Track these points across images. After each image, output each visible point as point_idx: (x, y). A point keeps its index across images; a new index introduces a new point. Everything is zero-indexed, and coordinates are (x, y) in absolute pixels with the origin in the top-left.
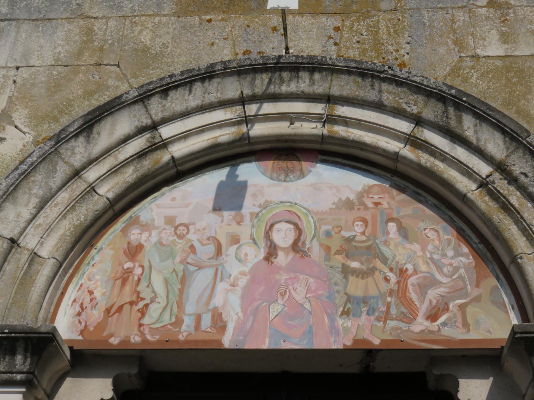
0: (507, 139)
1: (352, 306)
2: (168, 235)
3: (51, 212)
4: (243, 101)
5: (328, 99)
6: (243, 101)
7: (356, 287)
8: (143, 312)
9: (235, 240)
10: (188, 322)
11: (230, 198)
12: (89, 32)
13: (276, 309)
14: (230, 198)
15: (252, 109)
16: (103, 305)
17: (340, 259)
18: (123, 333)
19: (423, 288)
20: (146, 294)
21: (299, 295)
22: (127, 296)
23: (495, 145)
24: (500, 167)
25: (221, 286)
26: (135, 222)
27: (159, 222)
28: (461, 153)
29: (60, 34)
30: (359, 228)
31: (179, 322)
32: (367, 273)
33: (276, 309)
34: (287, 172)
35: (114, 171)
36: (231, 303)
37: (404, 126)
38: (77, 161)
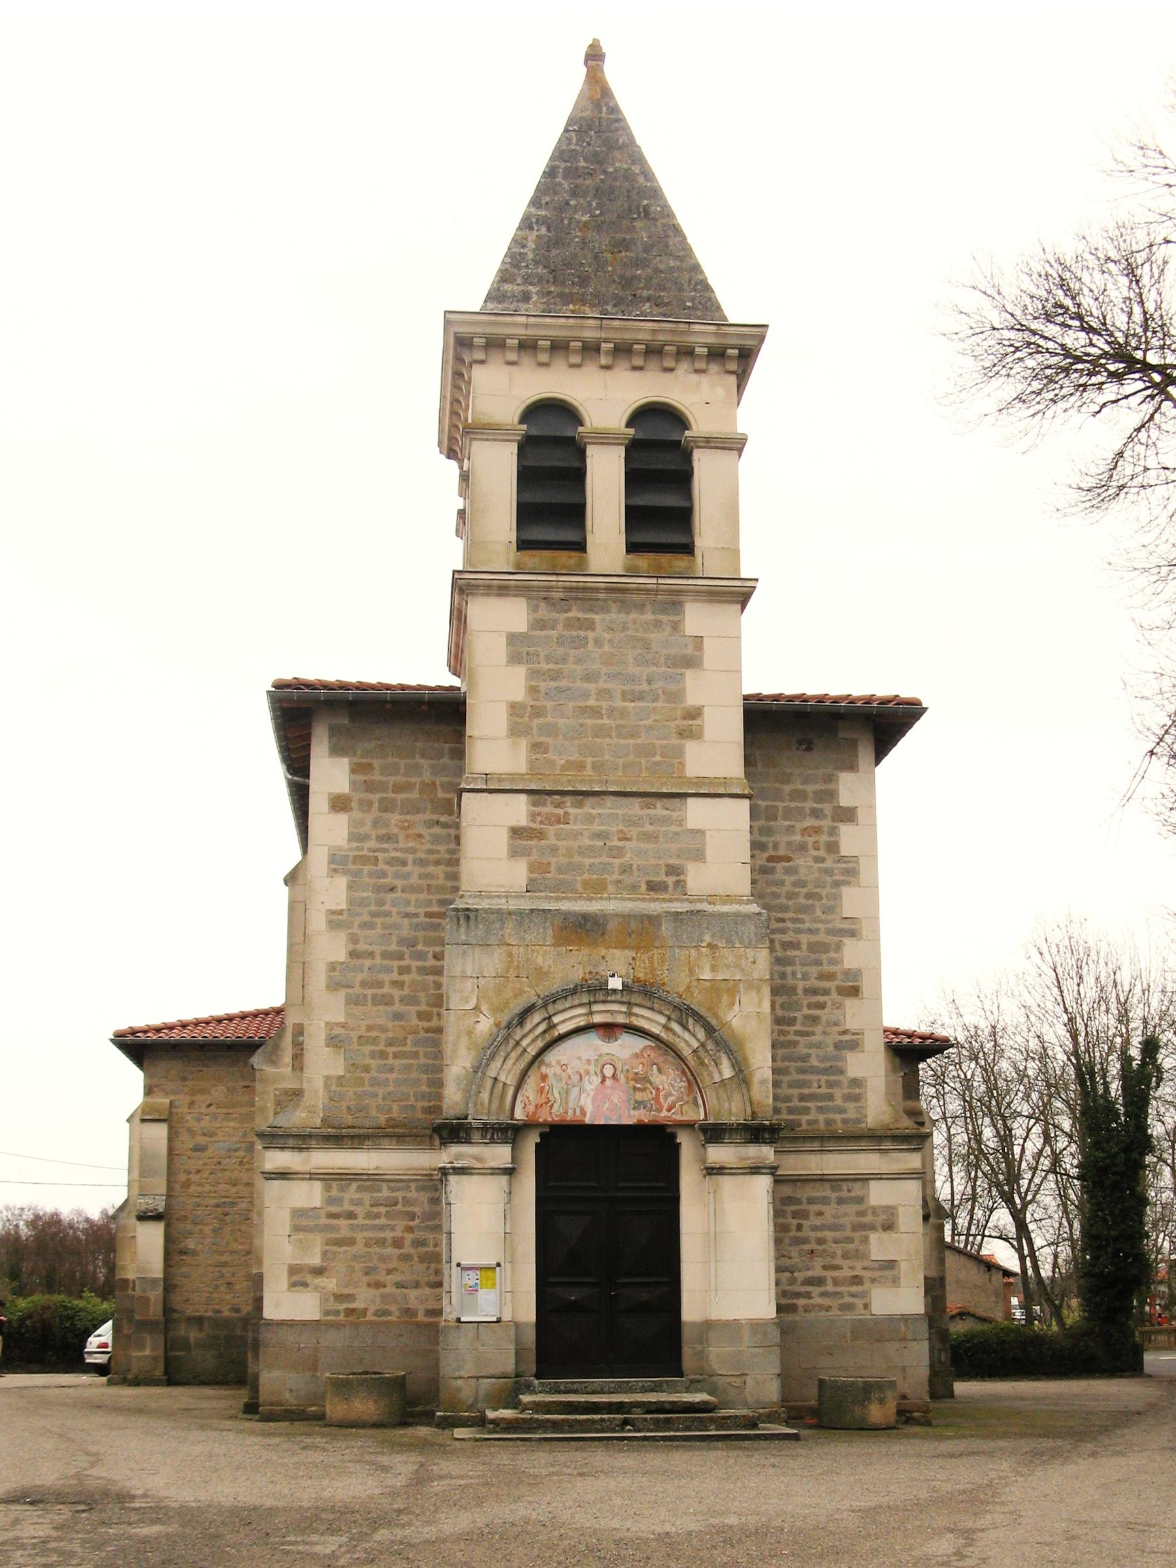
0: (841, 735)
1: (638, 1105)
2: (558, 1070)
3: (510, 1063)
7: (639, 1096)
9: (588, 1073)
12: (510, 955)
13: (606, 1106)
18: (544, 1116)
21: (616, 1101)
25: (583, 1096)
28: (686, 1035)
31: (566, 1112)
33: (606, 1106)
35: (534, 1040)
36: (587, 1103)
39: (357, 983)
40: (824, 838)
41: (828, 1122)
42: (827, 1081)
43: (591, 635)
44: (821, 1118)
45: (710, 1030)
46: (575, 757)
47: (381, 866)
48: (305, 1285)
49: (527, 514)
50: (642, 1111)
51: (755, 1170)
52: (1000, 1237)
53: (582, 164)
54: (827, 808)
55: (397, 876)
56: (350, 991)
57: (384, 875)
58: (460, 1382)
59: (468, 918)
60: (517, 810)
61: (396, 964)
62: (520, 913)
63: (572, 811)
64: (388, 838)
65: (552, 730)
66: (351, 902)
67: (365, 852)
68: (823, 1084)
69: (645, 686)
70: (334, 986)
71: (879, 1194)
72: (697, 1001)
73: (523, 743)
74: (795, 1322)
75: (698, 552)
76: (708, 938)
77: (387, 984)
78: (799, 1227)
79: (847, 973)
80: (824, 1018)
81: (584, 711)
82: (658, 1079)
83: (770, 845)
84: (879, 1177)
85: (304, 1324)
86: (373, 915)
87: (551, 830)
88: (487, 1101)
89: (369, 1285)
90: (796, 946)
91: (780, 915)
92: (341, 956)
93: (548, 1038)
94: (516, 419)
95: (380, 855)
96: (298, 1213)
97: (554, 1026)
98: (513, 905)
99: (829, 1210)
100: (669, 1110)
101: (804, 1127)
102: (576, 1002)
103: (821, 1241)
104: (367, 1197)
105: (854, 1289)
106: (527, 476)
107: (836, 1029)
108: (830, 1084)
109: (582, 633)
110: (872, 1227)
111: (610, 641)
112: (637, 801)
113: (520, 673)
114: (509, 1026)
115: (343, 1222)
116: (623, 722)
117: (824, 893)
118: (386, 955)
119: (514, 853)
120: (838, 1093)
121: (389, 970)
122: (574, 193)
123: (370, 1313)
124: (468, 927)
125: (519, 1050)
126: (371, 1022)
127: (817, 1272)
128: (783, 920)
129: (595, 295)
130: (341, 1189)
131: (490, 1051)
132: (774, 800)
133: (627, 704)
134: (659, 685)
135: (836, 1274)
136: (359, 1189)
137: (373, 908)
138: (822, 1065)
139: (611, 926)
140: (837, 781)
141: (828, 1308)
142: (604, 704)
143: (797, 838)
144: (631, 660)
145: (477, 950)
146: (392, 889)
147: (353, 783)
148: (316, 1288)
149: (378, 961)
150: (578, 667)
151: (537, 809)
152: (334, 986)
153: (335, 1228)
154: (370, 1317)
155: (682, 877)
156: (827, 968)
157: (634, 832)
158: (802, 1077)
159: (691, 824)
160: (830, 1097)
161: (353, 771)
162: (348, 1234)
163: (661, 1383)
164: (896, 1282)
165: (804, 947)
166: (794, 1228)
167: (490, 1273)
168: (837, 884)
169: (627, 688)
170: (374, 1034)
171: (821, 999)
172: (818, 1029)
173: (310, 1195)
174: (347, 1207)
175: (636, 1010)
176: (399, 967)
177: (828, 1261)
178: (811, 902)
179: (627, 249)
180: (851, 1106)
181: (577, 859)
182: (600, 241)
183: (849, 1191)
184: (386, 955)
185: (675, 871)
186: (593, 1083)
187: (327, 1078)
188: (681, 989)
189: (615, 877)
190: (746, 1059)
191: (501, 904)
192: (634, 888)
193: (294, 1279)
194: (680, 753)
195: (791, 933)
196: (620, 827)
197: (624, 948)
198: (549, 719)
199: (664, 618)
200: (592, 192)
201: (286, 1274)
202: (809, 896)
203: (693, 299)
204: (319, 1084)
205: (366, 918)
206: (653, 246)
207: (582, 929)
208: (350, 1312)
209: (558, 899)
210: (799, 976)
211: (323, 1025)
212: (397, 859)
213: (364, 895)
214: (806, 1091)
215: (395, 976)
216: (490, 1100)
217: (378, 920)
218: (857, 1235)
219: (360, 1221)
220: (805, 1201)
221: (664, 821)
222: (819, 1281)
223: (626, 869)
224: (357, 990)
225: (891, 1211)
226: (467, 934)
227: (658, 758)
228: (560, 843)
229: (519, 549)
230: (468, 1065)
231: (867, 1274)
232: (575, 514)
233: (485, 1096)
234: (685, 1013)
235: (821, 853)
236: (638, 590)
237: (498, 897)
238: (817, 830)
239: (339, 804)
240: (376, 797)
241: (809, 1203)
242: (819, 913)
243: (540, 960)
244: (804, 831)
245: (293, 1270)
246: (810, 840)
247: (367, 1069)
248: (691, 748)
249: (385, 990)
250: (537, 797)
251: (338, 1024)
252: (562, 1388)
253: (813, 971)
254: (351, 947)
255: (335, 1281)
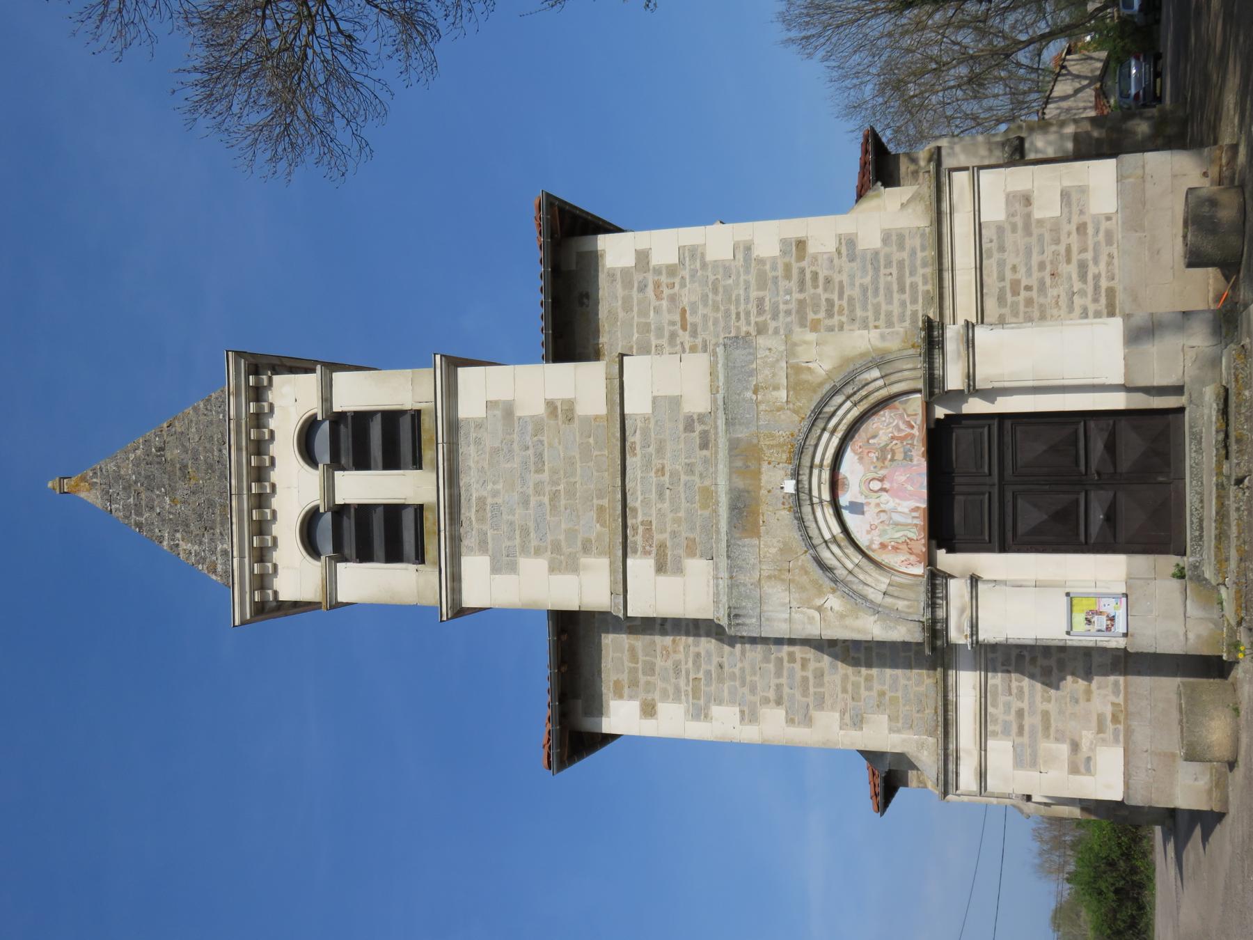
0: (574, 267)
1: (907, 457)
2: (876, 532)
3: (869, 580)
4: (812, 504)
5: (811, 467)
6: (812, 504)
7: (899, 456)
8: (911, 540)
9: (878, 505)
10: (915, 521)
11: (857, 508)
12: (769, 577)
13: (910, 488)
14: (857, 508)
15: (815, 500)
16: (908, 556)
17: (887, 463)
18: (921, 546)
19: (900, 430)
20: (903, 539)
21: (903, 478)
22: (904, 546)
23: (839, 399)
24: (848, 398)
25: (899, 509)
26: (869, 547)
27: (869, 537)
28: (840, 413)
29: (770, 591)
30: (872, 455)
31: (916, 525)
32: (893, 451)
33: (910, 488)
34: (844, 484)
35: (848, 556)
36: (906, 506)
37: (826, 435)
38: (845, 572)
39: (804, 699)
40: (664, 279)
41: (924, 265)
42: (885, 267)
43: (489, 501)
44: (921, 271)
45: (835, 391)
46: (593, 514)
47: (701, 675)
48: (1089, 759)
49: (394, 555)
50: (914, 453)
51: (970, 343)
52: (1039, 55)
53: (131, 500)
54: (637, 277)
55: (709, 661)
56: (811, 707)
57: (708, 673)
58: (1191, 636)
59: (736, 616)
60: (641, 567)
61: (786, 664)
62: (730, 569)
63: (640, 519)
64: (677, 671)
65: (571, 534)
66: (732, 702)
67: (690, 689)
68: (888, 271)
69: (531, 452)
70: (808, 721)
71: (994, 211)
72: (808, 404)
73: (584, 560)
74: (1125, 289)
75: (417, 406)
76: (749, 394)
77: (804, 674)
78: (1028, 288)
79: (784, 252)
80: (826, 273)
81: (554, 507)
82: (883, 438)
83: (672, 328)
84: (977, 212)
85: (1127, 764)
86: (743, 684)
87: (658, 537)
88: (906, 603)
89: (1088, 700)
90: (760, 302)
91: (734, 317)
92: (780, 713)
93: (844, 543)
94: (318, 564)
95: (692, 676)
96: (1019, 763)
97: (834, 537)
98: (724, 574)
99: (1011, 259)
100: (912, 427)
101: (929, 287)
102: (811, 517)
103: (1042, 266)
104: (1002, 699)
105: (1090, 231)
106: (364, 555)
107: (836, 261)
108: (889, 264)
109: (488, 508)
110: (1028, 216)
111: (494, 483)
112: (630, 460)
113: (525, 563)
114: (835, 581)
115: (1027, 722)
116: (562, 472)
117: (712, 278)
118: (779, 674)
119: (679, 570)
120: (897, 256)
121: (792, 671)
122: (152, 508)
123: (1117, 701)
124: (744, 616)
125: (856, 571)
126: (839, 689)
127: (1073, 269)
128: (738, 314)
129: (221, 494)
130: (995, 721)
131: (856, 598)
132: (632, 325)
133: (546, 468)
134: (529, 440)
135: (1075, 249)
136: (995, 706)
137: (737, 683)
138: (870, 273)
139: (740, 483)
140: (614, 269)
141: (1110, 256)
142: (547, 489)
143: (665, 303)
144: (508, 465)
145: (765, 608)
146: (721, 666)
147: (631, 698)
148: (1092, 749)
149: (784, 680)
150: (518, 511)
151: (640, 549)
152: (808, 721)
153: (1033, 727)
154: (1120, 700)
155: (695, 417)
156: (780, 272)
157: (656, 463)
158: (882, 292)
159: (647, 409)
160: (901, 264)
161: (621, 697)
162: (1039, 717)
163: (1192, 433)
164: (1083, 190)
165: (761, 294)
166: (1028, 294)
167: (1075, 601)
168: (704, 265)
169: (532, 468)
170: (850, 687)
171: (808, 276)
172: (837, 278)
173: (1001, 751)
174: (1012, 717)
175: (817, 461)
176: (789, 662)
177: (1062, 258)
178: (721, 290)
179: (186, 466)
180: (908, 243)
181: (681, 514)
182: (182, 488)
183: (991, 241)
184: (779, 674)
185: (689, 425)
186: (888, 494)
187: (891, 730)
188: (797, 418)
189: (696, 478)
190: (862, 355)
191: (723, 584)
192: (706, 461)
193: (1082, 770)
194: (586, 420)
195: (750, 306)
196: (653, 474)
197: (759, 472)
198: (562, 537)
199: (473, 435)
200: (149, 493)
201: (1078, 777)
202: (715, 291)
203: (218, 413)
204: (896, 738)
205: (746, 690)
206: (183, 445)
207: (744, 512)
208: (1115, 719)
209: (718, 532)
210: (788, 297)
211: (842, 732)
212: (694, 663)
213: (726, 691)
214: (895, 287)
215: (797, 666)
216: (904, 599)
217: (748, 678)
218: (1035, 231)
219: (1025, 705)
220: (1002, 284)
221: (646, 432)
222: (1083, 267)
223: (690, 469)
224: (810, 700)
225: (1011, 198)
226: (751, 617)
227: (591, 440)
228: (669, 530)
229: (423, 562)
230: (873, 618)
231: (1076, 219)
232: (393, 512)
233: (901, 604)
234: (819, 415)
235: (677, 281)
236: (449, 460)
237: (717, 586)
238: (657, 285)
239: (649, 710)
240: (642, 679)
241: (1003, 280)
242: (730, 281)
243: (773, 550)
244: (659, 297)
245: (1074, 770)
246: (666, 292)
247: (882, 694)
248: (583, 410)
249: (810, 675)
250: (629, 550)
251: (842, 719)
252: (1197, 533)
253: (783, 284)
254: (772, 704)
255: (1084, 732)
